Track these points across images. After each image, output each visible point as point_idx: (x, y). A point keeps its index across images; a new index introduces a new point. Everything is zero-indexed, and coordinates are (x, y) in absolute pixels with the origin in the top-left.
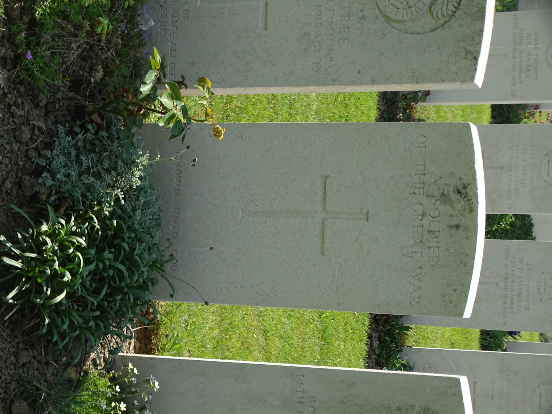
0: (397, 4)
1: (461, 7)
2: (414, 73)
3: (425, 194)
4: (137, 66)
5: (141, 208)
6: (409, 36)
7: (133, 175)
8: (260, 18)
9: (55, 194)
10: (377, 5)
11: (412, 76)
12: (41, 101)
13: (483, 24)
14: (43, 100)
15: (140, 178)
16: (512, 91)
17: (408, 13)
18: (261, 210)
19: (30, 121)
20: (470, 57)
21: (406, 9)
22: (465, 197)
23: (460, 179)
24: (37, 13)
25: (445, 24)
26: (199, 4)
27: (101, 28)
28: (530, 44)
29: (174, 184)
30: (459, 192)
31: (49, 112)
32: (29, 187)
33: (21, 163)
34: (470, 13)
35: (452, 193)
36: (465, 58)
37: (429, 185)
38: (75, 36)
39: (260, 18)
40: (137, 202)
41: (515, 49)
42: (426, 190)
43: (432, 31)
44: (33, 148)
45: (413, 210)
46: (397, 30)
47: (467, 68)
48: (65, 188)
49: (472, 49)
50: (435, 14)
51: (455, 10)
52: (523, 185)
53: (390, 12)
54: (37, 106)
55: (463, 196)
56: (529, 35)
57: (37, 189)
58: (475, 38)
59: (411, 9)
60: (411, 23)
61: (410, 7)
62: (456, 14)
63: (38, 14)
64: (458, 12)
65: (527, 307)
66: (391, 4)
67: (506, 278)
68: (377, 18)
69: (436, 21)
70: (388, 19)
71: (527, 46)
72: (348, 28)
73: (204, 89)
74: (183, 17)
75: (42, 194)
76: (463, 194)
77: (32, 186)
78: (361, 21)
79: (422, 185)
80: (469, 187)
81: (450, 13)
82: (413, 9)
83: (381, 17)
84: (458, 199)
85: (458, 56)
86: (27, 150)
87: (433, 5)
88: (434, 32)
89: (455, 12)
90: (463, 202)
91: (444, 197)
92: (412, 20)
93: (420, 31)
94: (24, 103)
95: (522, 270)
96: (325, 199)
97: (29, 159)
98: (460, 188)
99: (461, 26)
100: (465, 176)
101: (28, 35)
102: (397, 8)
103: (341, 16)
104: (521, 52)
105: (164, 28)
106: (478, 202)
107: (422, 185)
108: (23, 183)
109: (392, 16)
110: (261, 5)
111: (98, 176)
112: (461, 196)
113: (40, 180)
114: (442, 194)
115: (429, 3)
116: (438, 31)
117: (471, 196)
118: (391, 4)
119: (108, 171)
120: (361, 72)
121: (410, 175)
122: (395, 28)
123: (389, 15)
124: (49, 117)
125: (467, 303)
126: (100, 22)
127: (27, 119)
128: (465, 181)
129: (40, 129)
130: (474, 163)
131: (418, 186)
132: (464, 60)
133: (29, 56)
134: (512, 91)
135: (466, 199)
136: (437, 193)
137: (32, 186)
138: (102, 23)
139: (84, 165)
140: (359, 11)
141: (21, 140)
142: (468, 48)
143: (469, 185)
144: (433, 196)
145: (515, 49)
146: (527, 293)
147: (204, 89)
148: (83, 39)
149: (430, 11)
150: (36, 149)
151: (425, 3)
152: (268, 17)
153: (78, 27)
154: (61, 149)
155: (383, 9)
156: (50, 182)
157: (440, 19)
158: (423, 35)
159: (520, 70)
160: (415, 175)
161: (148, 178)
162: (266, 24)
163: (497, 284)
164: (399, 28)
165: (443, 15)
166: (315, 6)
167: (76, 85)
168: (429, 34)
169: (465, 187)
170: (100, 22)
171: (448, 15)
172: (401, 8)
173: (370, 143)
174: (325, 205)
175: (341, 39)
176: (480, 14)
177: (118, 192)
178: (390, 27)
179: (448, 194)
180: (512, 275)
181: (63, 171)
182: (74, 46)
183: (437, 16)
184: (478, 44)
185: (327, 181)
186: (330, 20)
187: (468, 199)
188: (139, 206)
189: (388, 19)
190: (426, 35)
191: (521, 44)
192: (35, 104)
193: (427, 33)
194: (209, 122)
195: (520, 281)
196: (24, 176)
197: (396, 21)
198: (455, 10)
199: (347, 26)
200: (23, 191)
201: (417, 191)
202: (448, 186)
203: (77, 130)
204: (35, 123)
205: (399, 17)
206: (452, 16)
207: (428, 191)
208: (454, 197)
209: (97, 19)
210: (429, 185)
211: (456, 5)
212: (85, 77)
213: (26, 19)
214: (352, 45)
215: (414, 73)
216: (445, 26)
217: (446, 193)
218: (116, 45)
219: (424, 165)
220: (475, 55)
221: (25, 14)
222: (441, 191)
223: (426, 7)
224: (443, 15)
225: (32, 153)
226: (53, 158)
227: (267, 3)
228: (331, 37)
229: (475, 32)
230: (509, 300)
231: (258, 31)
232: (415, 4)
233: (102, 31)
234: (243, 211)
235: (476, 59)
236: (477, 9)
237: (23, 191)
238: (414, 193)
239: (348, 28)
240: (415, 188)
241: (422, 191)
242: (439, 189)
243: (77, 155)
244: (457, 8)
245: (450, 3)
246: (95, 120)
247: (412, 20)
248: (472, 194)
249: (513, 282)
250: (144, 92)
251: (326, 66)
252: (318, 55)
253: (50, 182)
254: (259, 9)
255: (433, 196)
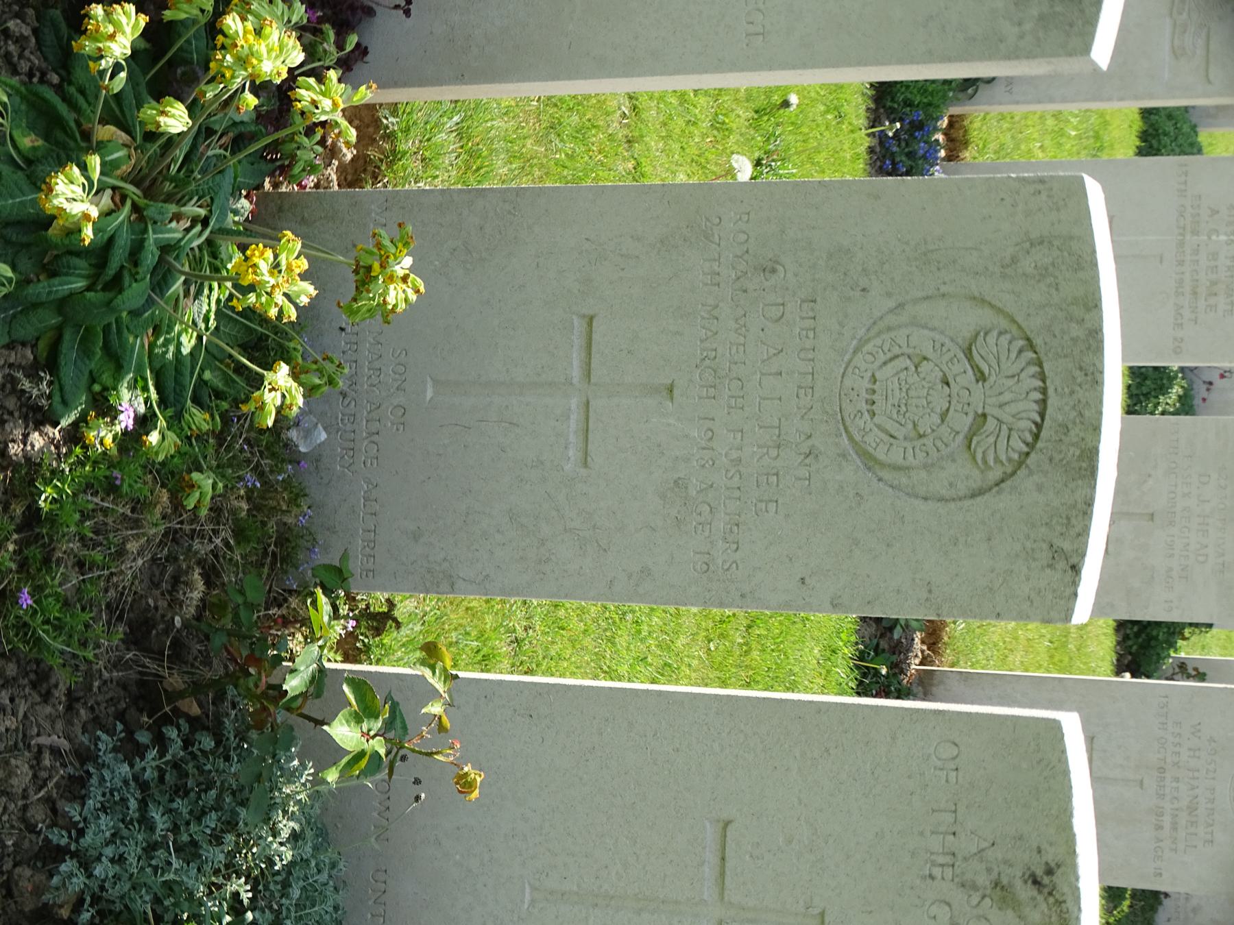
0: (891, 426)
1: (1039, 445)
2: (930, 591)
3: (956, 880)
4: (288, 540)
5: (293, 914)
6: (918, 503)
7: (275, 833)
8: (572, 438)
9: (91, 905)
10: (844, 424)
11: (927, 599)
12: (56, 686)
13: (1093, 488)
14: (63, 680)
15: (295, 837)
16: (1175, 339)
17: (917, 451)
18: (575, 888)
19: (32, 737)
20: (1061, 565)
21: (911, 440)
22: (1050, 894)
23: (1039, 852)
24: (43, 497)
25: (1003, 481)
26: (429, 394)
27: (197, 495)
28: (1217, 232)
29: (375, 814)
30: (1036, 882)
31: (78, 700)
32: (31, 893)
33: (10, 843)
34: (1061, 460)
35: (1018, 883)
36: (1050, 566)
37: (965, 859)
38: (136, 524)
39: (572, 438)
40: (284, 901)
41: (1181, 244)
42: (958, 871)
43: (973, 496)
44: (39, 800)
45: (929, 917)
46: (891, 486)
47: (1054, 591)
48: (113, 892)
49: (1066, 546)
50: (979, 456)
51: (1025, 449)
52: (1201, 559)
53: (874, 445)
54: (46, 697)
55: (1046, 891)
56: (1215, 212)
57: (47, 897)
58: (1073, 521)
59: (924, 440)
60: (923, 474)
61: (921, 436)
62: (1028, 461)
63: (45, 500)
64: (1033, 455)
65: (1209, 837)
66: (879, 427)
67: (1162, 770)
68: (844, 456)
69: (982, 472)
70: (869, 460)
71: (1210, 238)
72: (777, 474)
73: (434, 673)
74: (393, 424)
75: (61, 906)
76: (1045, 886)
77: (38, 891)
78: (807, 461)
79: (948, 859)
80: (1059, 872)
81: (1016, 456)
82: (928, 441)
83: (855, 456)
84: (1034, 899)
85: (1034, 559)
86: (25, 808)
87: (974, 434)
88: (979, 499)
89: (1028, 454)
90: (1044, 907)
91: (1001, 891)
92: (925, 466)
93: (944, 492)
94: (17, 700)
95: (1197, 754)
96: (722, 874)
97: (31, 828)
98: (1039, 872)
99: (1040, 488)
100: (1051, 844)
101: (22, 545)
102: (892, 436)
103: (759, 447)
104: (1196, 252)
105: (351, 445)
106: (1079, 909)
107: (948, 859)
108: (17, 885)
109: (881, 456)
110: (573, 407)
111: (190, 851)
112: (1040, 892)
113: (55, 880)
114: (996, 884)
115: (966, 429)
116: (986, 496)
117: (1063, 894)
118: (879, 427)
119: (216, 839)
120: (807, 581)
121: (922, 834)
122: (886, 483)
123: (871, 450)
124: (78, 713)
125: (1074, 791)
126: (193, 486)
127: (24, 735)
128: (1050, 856)
129: (55, 751)
130: (1071, 816)
131: (941, 860)
132: (1048, 571)
133: (26, 600)
134: (1175, 339)
135: (1051, 900)
136: (983, 880)
137: (38, 891)
138: (199, 487)
139: (158, 830)
140: (803, 437)
141: (9, 790)
142: (1058, 542)
143: (1058, 866)
144: (974, 887)
145: (1181, 244)
146: (1209, 806)
147: (434, 673)
148: (155, 528)
149: (969, 447)
150: (49, 801)
151: (958, 429)
152: (590, 436)
153: (139, 505)
154: (104, 795)
155: (858, 438)
156: (79, 882)
157: (990, 468)
158: (952, 505)
159: (1195, 293)
160: (933, 833)
161: (309, 834)
162: (586, 454)
163: (1141, 783)
164: (896, 482)
165: (997, 460)
166: (700, 418)
167: (141, 629)
168: (967, 503)
169: (1050, 872)
170: (193, 486)
171: (1010, 460)
172: (901, 437)
173: (827, 750)
174: (723, 889)
175: (761, 501)
176: (1084, 465)
177: (240, 886)
178: (875, 480)
179: (1011, 885)
180: (1176, 764)
181: (109, 851)
182: (133, 546)
183: (985, 461)
184: (1079, 535)
185: (728, 834)
186: (735, 454)
187: (1057, 901)
188: (288, 909)
189: (869, 460)
190: (959, 504)
191: (1195, 233)
192: (43, 692)
193: (960, 499)
194: (448, 755)
195: (1194, 778)
196: (18, 870)
197: (889, 466)
198: (1025, 449)
199: (775, 471)
200: (16, 902)
201: (937, 872)
202: (1011, 866)
203: (143, 737)
204: (43, 740)
205: (896, 456)
206: (1020, 464)
207: (963, 873)
208: (1025, 892)
209: (187, 478)
210: (965, 859)
211: (1029, 439)
212: (160, 612)
213: (18, 510)
214: (787, 516)
215: (930, 591)
216: (1003, 485)
217: (1005, 881)
218: (234, 512)
219: (955, 811)
220: (1074, 560)
221: (15, 496)
222: (994, 876)
223: (961, 437)
224: (997, 460)
225: (38, 814)
226: (85, 820)
227: (588, 402)
228: (737, 494)
229: (1074, 506)
230: (1167, 820)
231: (568, 467)
232: (933, 431)
233: (199, 501)
234: (534, 889)
235: (1076, 569)
236: (1078, 453)
237: (16, 902)
238: (932, 877)
239: (777, 474)
240: (934, 864)
241: (949, 872)
242: (989, 870)
243: (143, 804)
244: (1031, 446)
245: (1015, 434)
246: (186, 710)
247: (925, 466)
248: (1066, 889)
249: (1177, 780)
250: (293, 689)
251: (724, 561)
252: (707, 534)
253: (79, 882)
254: (569, 418)
255: (974, 887)
